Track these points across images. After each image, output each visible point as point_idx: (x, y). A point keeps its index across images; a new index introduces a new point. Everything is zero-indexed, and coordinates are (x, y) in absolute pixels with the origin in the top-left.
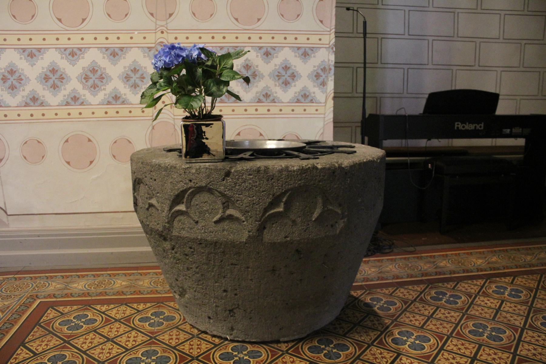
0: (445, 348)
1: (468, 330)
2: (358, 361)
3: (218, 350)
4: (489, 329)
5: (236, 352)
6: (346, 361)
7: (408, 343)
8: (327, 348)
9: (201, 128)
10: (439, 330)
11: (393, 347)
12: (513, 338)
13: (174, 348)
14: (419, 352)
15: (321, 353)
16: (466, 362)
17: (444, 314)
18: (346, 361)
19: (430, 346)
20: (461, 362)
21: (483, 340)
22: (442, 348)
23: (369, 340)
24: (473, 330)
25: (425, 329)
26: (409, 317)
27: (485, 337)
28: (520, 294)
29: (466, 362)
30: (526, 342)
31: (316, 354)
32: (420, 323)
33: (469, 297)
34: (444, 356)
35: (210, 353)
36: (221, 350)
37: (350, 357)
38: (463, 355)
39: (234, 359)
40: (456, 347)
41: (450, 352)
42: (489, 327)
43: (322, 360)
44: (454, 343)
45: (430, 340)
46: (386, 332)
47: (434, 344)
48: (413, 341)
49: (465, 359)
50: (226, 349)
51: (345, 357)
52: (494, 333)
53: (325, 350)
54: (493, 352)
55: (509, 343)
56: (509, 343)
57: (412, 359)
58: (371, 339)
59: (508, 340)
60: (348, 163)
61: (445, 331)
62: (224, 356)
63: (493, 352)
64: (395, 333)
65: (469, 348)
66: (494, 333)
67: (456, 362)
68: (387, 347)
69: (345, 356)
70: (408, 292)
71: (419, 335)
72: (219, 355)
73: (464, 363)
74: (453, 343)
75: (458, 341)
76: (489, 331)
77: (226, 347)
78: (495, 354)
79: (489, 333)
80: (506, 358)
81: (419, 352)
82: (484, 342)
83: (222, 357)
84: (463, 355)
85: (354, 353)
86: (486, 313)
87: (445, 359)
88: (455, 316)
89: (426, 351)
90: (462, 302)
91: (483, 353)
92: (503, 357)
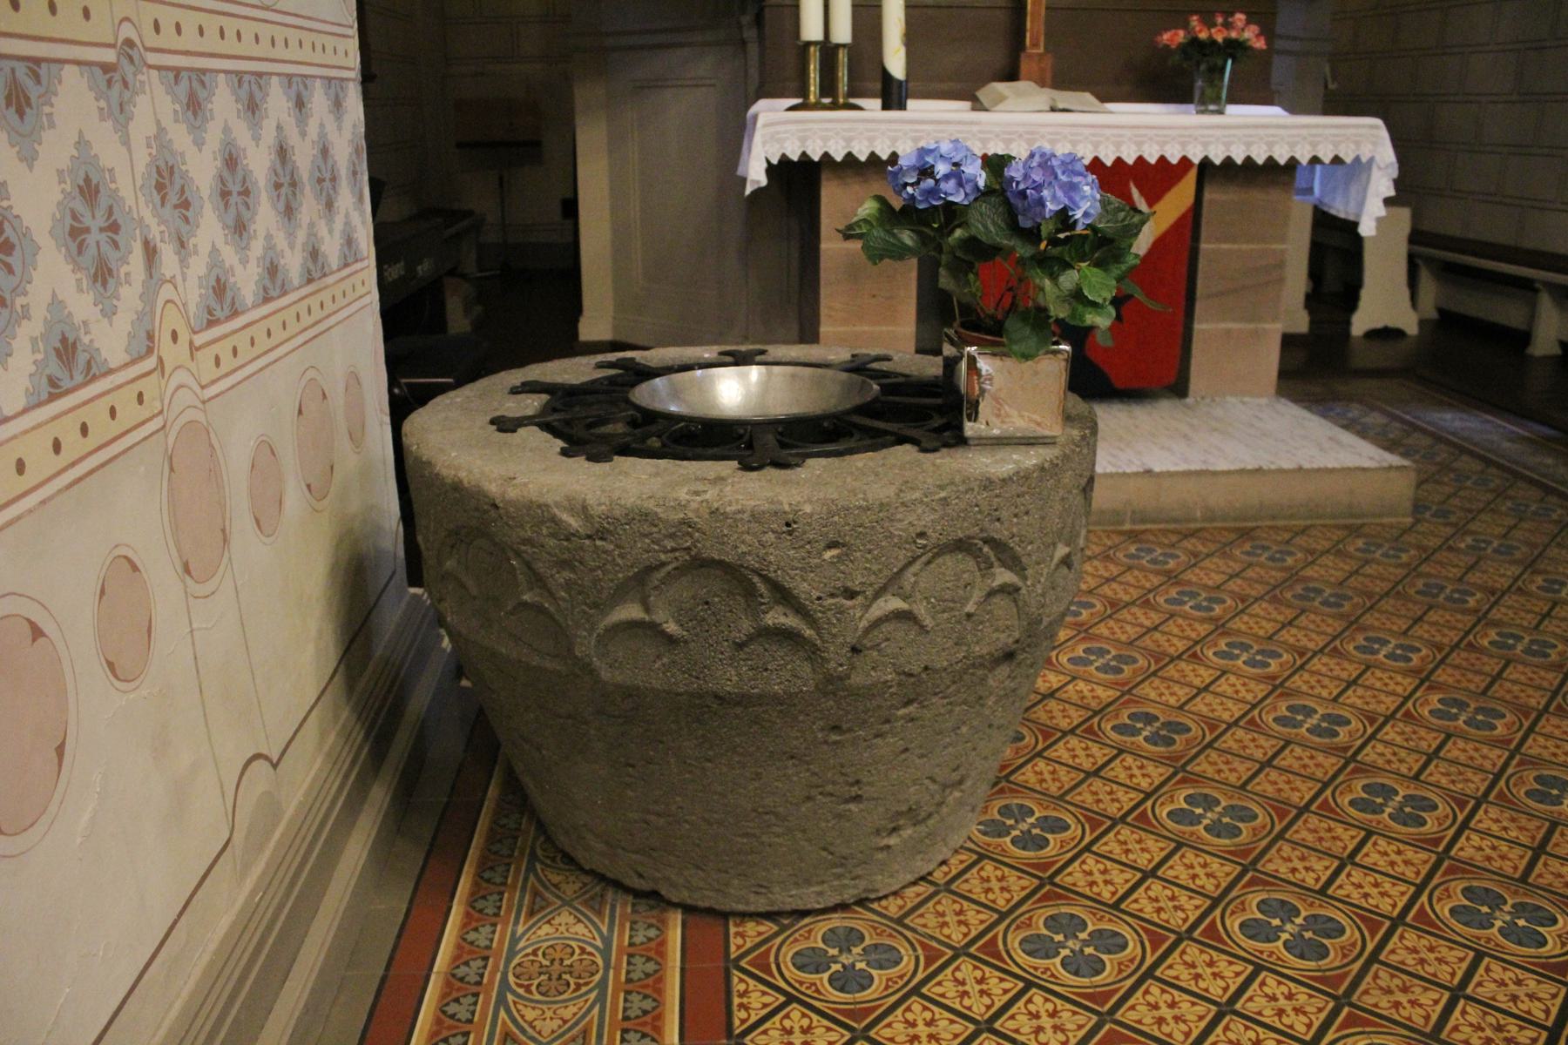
0: (1382, 957)
1: (1450, 905)
2: (1150, 981)
3: (788, 942)
4: (1507, 908)
5: (834, 947)
6: (1120, 981)
7: (1285, 936)
8: (1070, 943)
9: (908, 74)
10: (1370, 901)
11: (1243, 945)
12: (1436, 893)
13: (791, 999)
14: (1312, 964)
15: (1054, 957)
16: (1535, 1040)
17: (1386, 854)
18: (1120, 981)
19: (1342, 948)
20: (1521, 1040)
21: (1489, 940)
22: (1374, 958)
23: (1180, 922)
24: (1464, 906)
25: (1470, 948)
26: (1290, 860)
27: (1495, 930)
28: (1539, 787)
29: (1535, 1040)
30: (1405, 881)
31: (1042, 958)
32: (1317, 880)
33: (1458, 805)
34: (1378, 981)
35: (769, 950)
36: (796, 940)
37: (1129, 971)
38: (1526, 1020)
39: (829, 968)
40: (1414, 956)
41: (1432, 982)
42: (1510, 902)
43: (1057, 978)
44: (1409, 944)
45: (1342, 931)
46: (1226, 900)
47: (1354, 945)
48: (1288, 927)
49: (1531, 1033)
50: (888, 980)
51: (1115, 972)
52: (1521, 922)
53: (1064, 947)
54: (1513, 976)
55: (1560, 956)
56: (1560, 956)
57: (1292, 985)
58: (1185, 920)
59: (1559, 946)
60: (27, 234)
61: (1385, 906)
62: (805, 960)
63: (1513, 976)
64: (1250, 905)
65: (1449, 959)
66: (1521, 922)
67: (1506, 1039)
68: (1226, 944)
69: (1116, 968)
70: (1289, 782)
71: (1313, 916)
72: (792, 958)
73: (1528, 1041)
74: (1405, 942)
75: (1419, 937)
76: (1509, 913)
77: (810, 932)
78: (1519, 982)
79: (1508, 918)
80: (1548, 997)
81: (1313, 964)
82: (1491, 945)
83: (799, 961)
84: (1526, 1020)
85: (1138, 958)
86: (1503, 857)
87: (1381, 988)
88: (1416, 861)
89: (1331, 962)
90: (1351, 791)
91: (1486, 978)
92: (1541, 995)
